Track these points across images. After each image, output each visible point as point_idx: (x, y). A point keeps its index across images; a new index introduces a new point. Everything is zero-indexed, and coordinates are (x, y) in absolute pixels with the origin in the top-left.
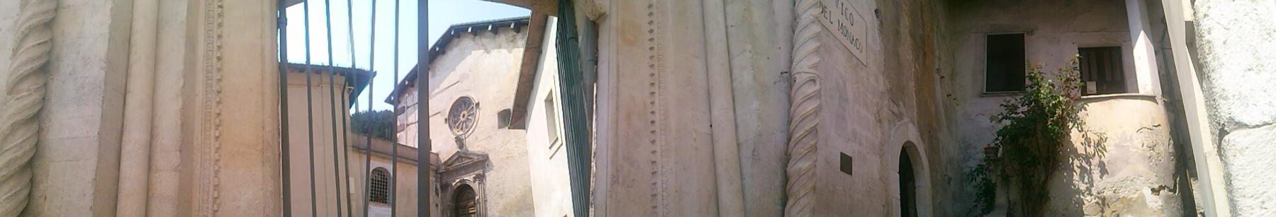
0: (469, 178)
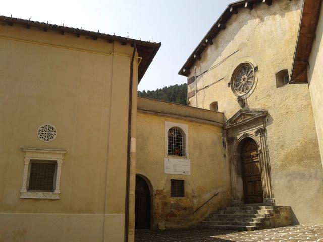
0: (251, 132)
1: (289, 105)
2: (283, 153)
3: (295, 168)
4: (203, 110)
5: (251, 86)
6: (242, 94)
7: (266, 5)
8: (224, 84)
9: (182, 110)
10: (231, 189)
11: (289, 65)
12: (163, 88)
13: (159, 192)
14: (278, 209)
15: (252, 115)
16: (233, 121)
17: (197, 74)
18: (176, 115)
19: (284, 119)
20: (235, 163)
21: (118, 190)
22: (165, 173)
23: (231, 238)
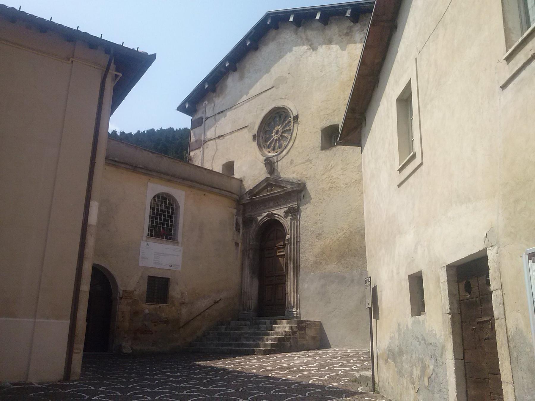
0: (279, 212)
1: (335, 177)
2: (319, 246)
3: (332, 267)
4: (211, 172)
5: (285, 143)
6: (272, 154)
7: (319, 24)
8: (247, 135)
9: (179, 168)
10: (241, 294)
11: (339, 119)
12: (148, 131)
13: (128, 294)
14: (304, 324)
15: (283, 187)
16: (255, 192)
17: (208, 115)
18: (168, 174)
19: (325, 197)
20: (251, 256)
21: (61, 282)
22: (140, 264)
23: (232, 364)
